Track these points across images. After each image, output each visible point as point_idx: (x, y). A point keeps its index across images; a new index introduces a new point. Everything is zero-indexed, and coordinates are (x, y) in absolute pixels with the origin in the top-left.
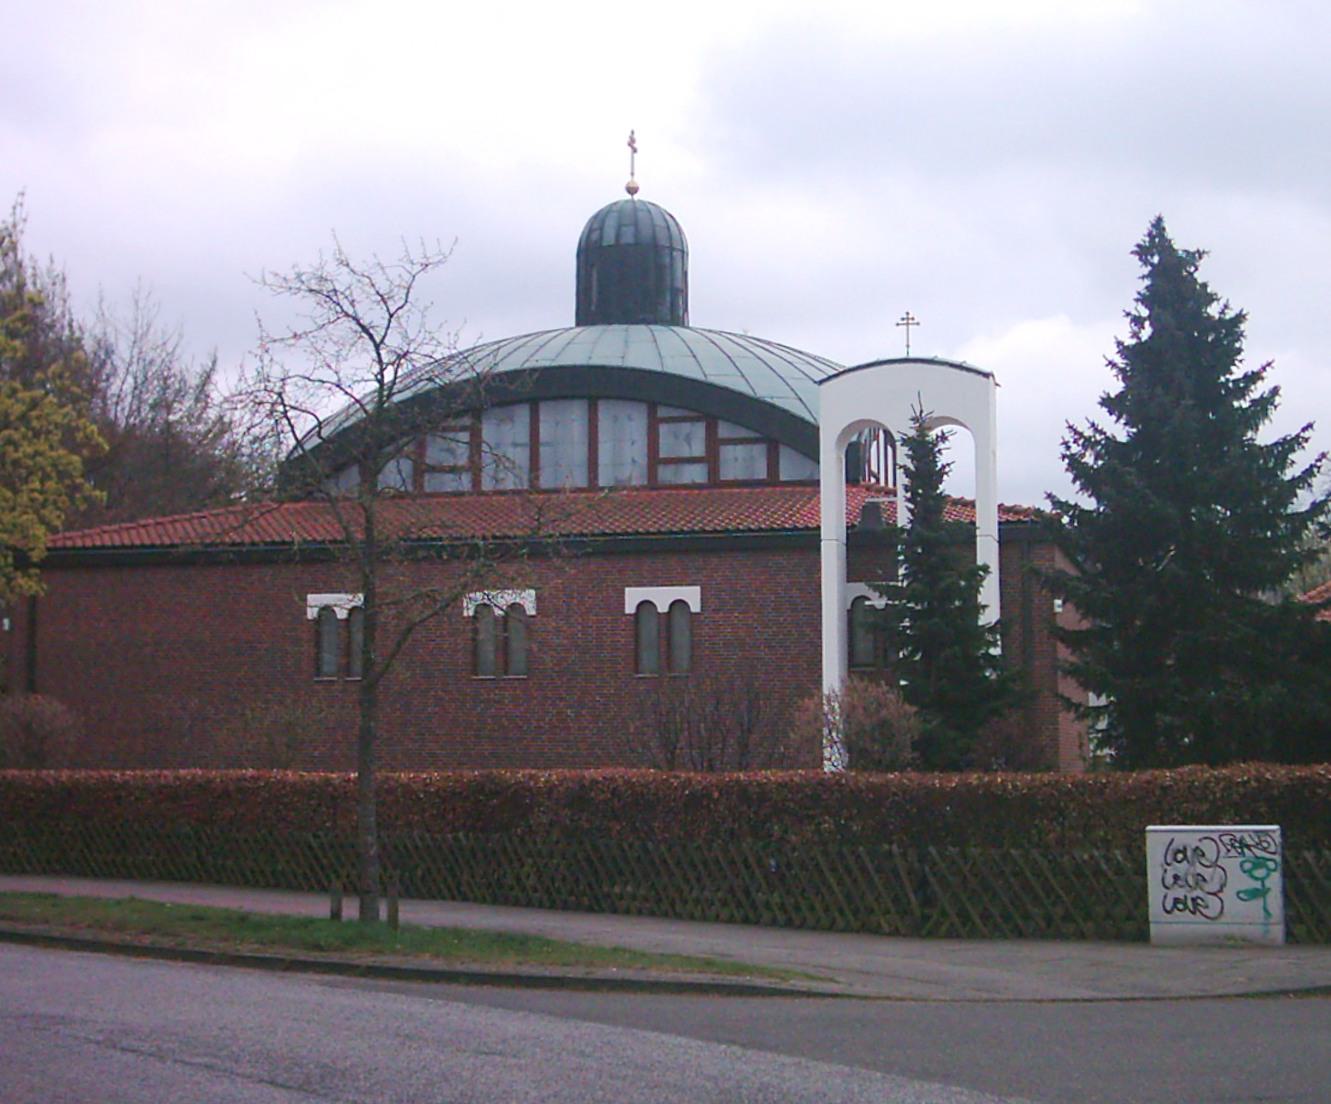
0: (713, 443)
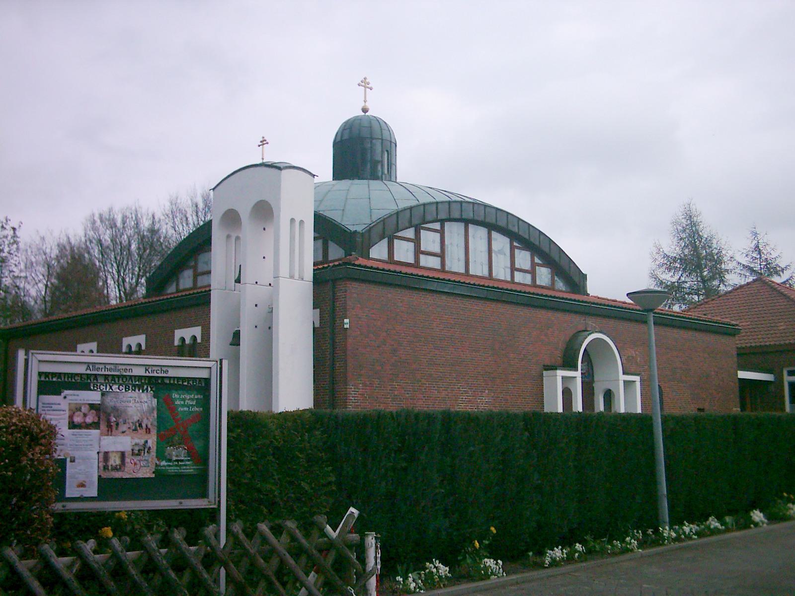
0: (534, 265)
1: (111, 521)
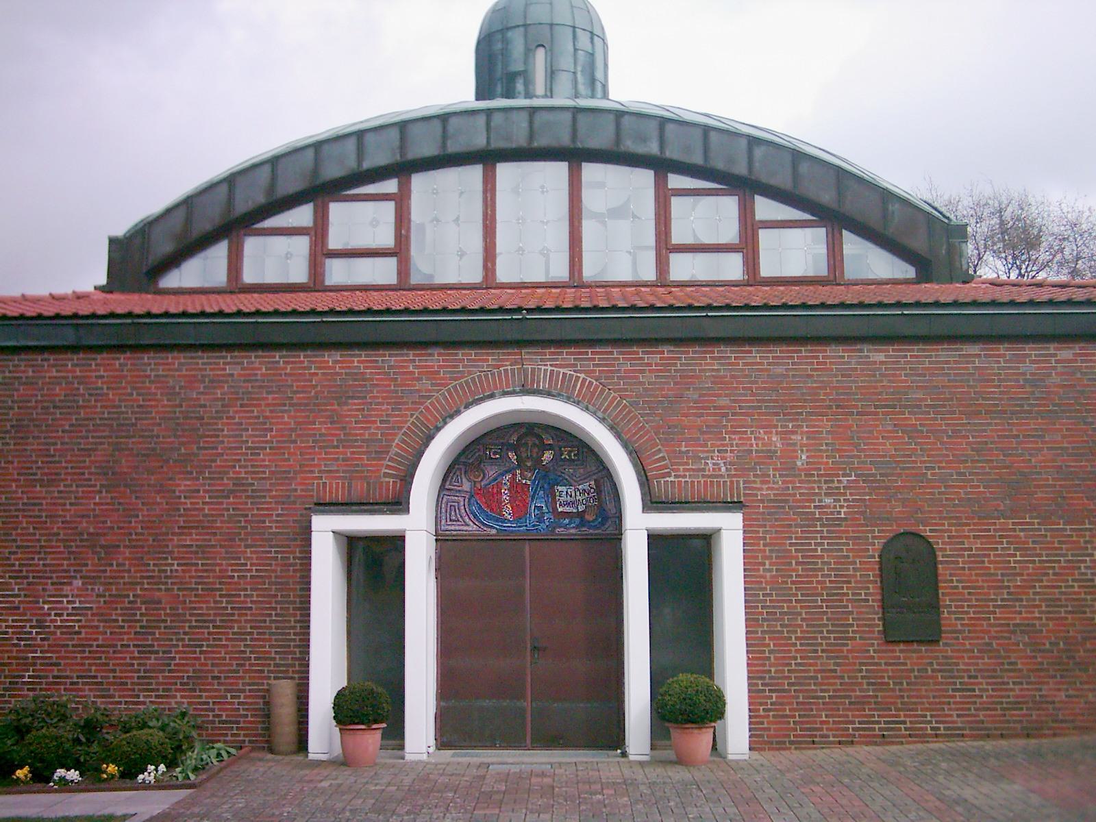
1: (107, 768)
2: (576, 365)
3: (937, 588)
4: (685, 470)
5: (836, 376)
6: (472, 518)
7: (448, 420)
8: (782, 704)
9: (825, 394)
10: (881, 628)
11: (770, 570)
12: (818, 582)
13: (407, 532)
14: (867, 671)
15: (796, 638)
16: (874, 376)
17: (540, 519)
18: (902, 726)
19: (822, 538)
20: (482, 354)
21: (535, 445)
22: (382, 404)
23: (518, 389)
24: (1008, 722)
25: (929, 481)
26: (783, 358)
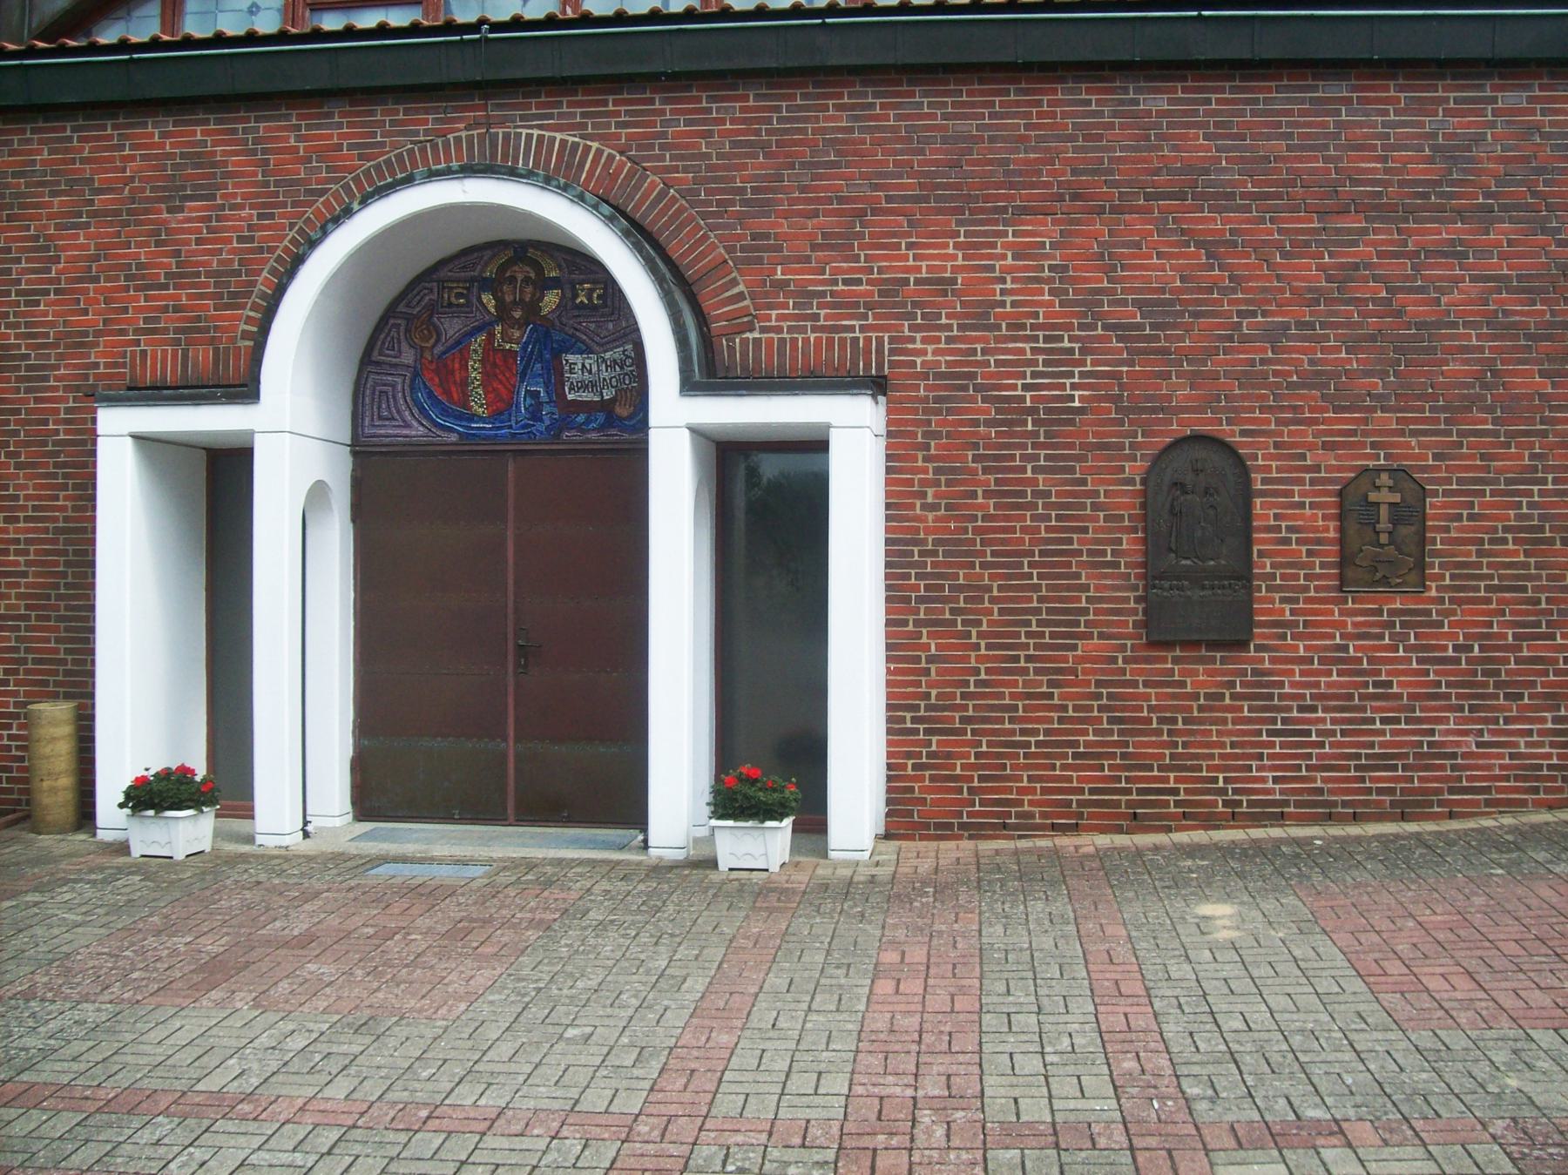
2: (584, 126)
3: (1248, 542)
4: (780, 318)
5: (1072, 138)
6: (415, 411)
7: (330, 226)
8: (949, 755)
9: (1052, 173)
10: (1140, 617)
11: (934, 507)
12: (1024, 530)
13: (257, 436)
14: (1110, 696)
15: (980, 635)
16: (1147, 138)
17: (535, 415)
18: (1171, 798)
19: (1035, 446)
20: (417, 111)
21: (527, 280)
22: (242, 207)
23: (455, 164)
24: (1369, 791)
25: (1245, 339)
26: (973, 105)
